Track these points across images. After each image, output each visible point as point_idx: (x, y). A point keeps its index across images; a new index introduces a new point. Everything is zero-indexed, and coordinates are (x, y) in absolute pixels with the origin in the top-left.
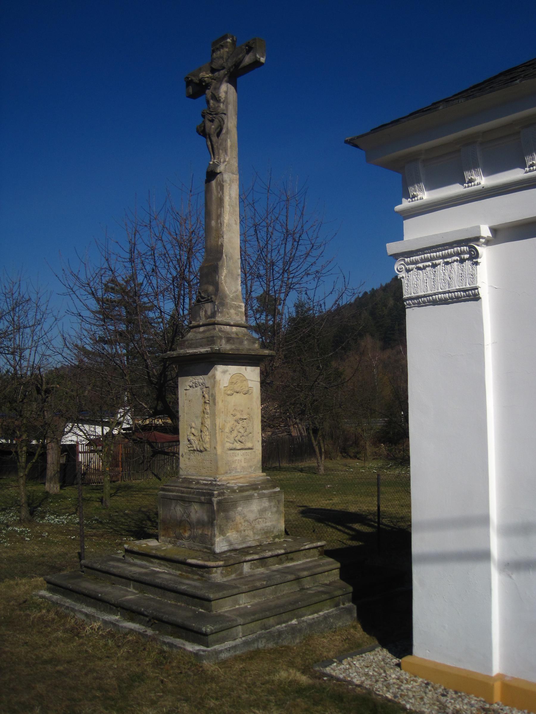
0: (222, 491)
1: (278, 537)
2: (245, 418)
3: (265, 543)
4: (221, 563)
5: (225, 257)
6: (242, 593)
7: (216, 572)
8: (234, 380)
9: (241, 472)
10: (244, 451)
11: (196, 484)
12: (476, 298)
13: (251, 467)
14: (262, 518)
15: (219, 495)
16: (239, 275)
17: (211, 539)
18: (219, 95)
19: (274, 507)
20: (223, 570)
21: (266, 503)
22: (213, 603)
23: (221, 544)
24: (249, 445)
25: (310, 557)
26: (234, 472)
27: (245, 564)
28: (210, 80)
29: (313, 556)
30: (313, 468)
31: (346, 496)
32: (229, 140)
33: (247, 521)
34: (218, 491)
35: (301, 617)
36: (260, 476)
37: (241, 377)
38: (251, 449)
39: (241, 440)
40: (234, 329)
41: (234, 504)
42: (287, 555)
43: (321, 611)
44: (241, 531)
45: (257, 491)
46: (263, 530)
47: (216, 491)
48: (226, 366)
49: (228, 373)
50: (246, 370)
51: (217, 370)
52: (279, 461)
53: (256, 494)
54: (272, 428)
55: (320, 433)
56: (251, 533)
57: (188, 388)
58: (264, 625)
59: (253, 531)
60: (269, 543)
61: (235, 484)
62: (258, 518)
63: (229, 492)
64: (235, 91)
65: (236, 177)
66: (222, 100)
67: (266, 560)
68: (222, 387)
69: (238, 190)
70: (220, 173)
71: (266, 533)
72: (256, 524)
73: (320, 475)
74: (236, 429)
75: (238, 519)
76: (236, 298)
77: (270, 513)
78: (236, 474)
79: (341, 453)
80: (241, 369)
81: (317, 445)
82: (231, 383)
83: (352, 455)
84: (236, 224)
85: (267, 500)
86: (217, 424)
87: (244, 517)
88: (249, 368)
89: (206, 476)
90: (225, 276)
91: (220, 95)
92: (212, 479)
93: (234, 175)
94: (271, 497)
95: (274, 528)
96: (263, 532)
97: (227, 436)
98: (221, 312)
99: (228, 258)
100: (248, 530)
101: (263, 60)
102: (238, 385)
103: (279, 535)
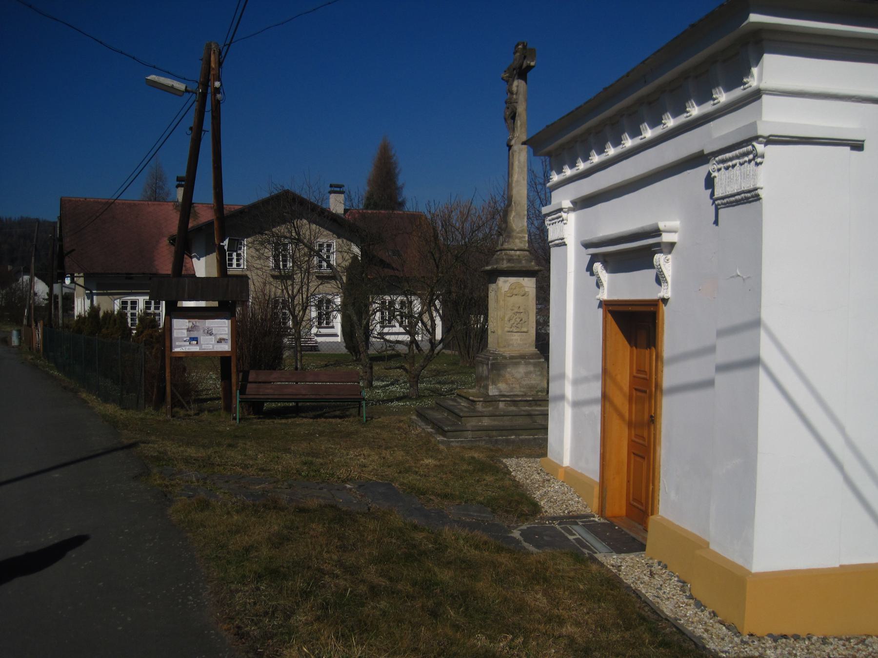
1: (541, 391)
2: (521, 311)
4: (481, 399)
6: (485, 416)
7: (479, 404)
9: (517, 347)
10: (519, 334)
12: (565, 244)
13: (526, 344)
15: (493, 359)
20: (483, 404)
21: (531, 368)
22: (463, 418)
24: (525, 330)
27: (500, 402)
32: (519, 121)
35: (519, 435)
38: (526, 332)
40: (518, 253)
41: (505, 366)
43: (536, 435)
44: (509, 384)
45: (525, 360)
49: (508, 282)
50: (523, 280)
56: (518, 386)
61: (509, 354)
64: (525, 84)
66: (514, 93)
67: (518, 403)
68: (503, 291)
70: (403, 184)
75: (507, 376)
76: (522, 231)
77: (534, 375)
80: (520, 280)
82: (510, 289)
88: (526, 279)
90: (514, 217)
92: (494, 350)
98: (507, 242)
99: (516, 205)
101: (532, 64)
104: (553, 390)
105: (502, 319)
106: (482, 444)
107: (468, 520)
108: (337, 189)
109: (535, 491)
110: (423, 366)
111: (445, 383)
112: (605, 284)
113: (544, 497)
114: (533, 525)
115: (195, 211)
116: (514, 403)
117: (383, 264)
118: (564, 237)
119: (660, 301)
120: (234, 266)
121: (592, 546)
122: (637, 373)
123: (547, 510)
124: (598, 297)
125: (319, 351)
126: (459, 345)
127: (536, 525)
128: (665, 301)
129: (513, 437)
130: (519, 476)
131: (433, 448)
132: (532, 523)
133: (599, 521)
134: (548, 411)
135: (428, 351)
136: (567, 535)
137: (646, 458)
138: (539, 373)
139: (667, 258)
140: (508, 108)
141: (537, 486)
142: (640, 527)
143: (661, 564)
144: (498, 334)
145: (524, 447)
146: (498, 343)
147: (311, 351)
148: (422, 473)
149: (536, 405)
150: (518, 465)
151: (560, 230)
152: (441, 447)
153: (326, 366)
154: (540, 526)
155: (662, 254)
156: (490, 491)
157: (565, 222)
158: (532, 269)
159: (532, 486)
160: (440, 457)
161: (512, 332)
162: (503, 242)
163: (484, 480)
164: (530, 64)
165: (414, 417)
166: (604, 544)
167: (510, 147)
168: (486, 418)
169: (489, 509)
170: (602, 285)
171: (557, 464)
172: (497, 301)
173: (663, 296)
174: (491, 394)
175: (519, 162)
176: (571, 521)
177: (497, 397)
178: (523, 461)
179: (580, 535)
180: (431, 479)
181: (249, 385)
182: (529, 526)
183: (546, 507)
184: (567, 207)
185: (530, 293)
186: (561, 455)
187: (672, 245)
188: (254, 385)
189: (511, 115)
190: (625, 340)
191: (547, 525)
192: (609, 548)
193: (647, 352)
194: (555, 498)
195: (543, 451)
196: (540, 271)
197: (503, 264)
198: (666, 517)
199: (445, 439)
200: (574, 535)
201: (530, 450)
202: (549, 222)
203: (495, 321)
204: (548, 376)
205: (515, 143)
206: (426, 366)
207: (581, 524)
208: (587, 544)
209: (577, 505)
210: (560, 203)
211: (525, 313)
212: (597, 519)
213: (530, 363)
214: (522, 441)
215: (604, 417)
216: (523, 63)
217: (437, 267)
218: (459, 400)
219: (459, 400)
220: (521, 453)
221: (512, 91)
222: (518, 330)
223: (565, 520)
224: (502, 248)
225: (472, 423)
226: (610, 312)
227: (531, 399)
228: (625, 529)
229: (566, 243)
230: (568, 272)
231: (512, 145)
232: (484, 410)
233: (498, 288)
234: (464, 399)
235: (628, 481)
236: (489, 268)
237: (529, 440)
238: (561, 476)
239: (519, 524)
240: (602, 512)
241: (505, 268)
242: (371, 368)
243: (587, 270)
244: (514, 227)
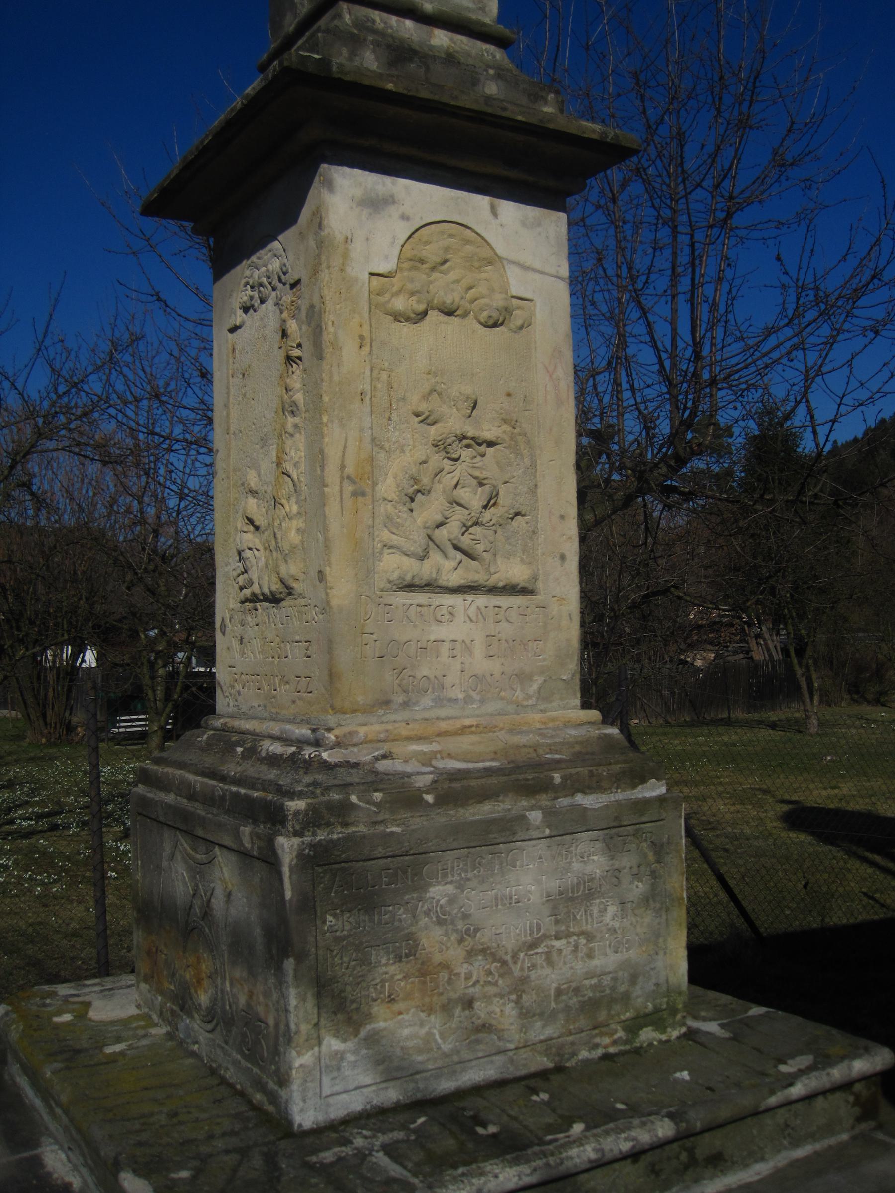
0: (335, 796)
2: (488, 435)
3: (584, 1054)
8: (431, 253)
9: (468, 700)
10: (482, 601)
11: (245, 756)
13: (523, 678)
14: (568, 935)
17: (276, 1052)
19: (636, 876)
23: (326, 1080)
25: (812, 1137)
26: (426, 701)
29: (829, 1129)
30: (797, 721)
31: (869, 781)
33: (483, 951)
34: (313, 795)
36: (568, 724)
37: (468, 242)
38: (525, 591)
39: (466, 541)
40: (441, 38)
42: (688, 1143)
45: (544, 800)
46: (577, 990)
47: (300, 795)
48: (388, 180)
49: (394, 211)
51: (329, 185)
52: (729, 707)
53: (535, 816)
54: (716, 645)
55: (809, 652)
57: (239, 316)
59: (517, 1002)
60: (606, 1057)
61: (427, 759)
62: (546, 937)
63: (378, 805)
68: (359, 271)
71: (591, 1006)
72: (534, 966)
73: (812, 735)
74: (438, 487)
77: (612, 909)
78: (443, 713)
79: (849, 692)
81: (803, 675)
83: (870, 697)
85: (598, 845)
86: (333, 454)
87: (472, 932)
88: (510, 210)
89: (290, 722)
92: (304, 731)
95: (634, 980)
96: (574, 1001)
97: (389, 518)
100: (487, 998)
102: (452, 276)
103: (657, 1010)
161: (430, 586)
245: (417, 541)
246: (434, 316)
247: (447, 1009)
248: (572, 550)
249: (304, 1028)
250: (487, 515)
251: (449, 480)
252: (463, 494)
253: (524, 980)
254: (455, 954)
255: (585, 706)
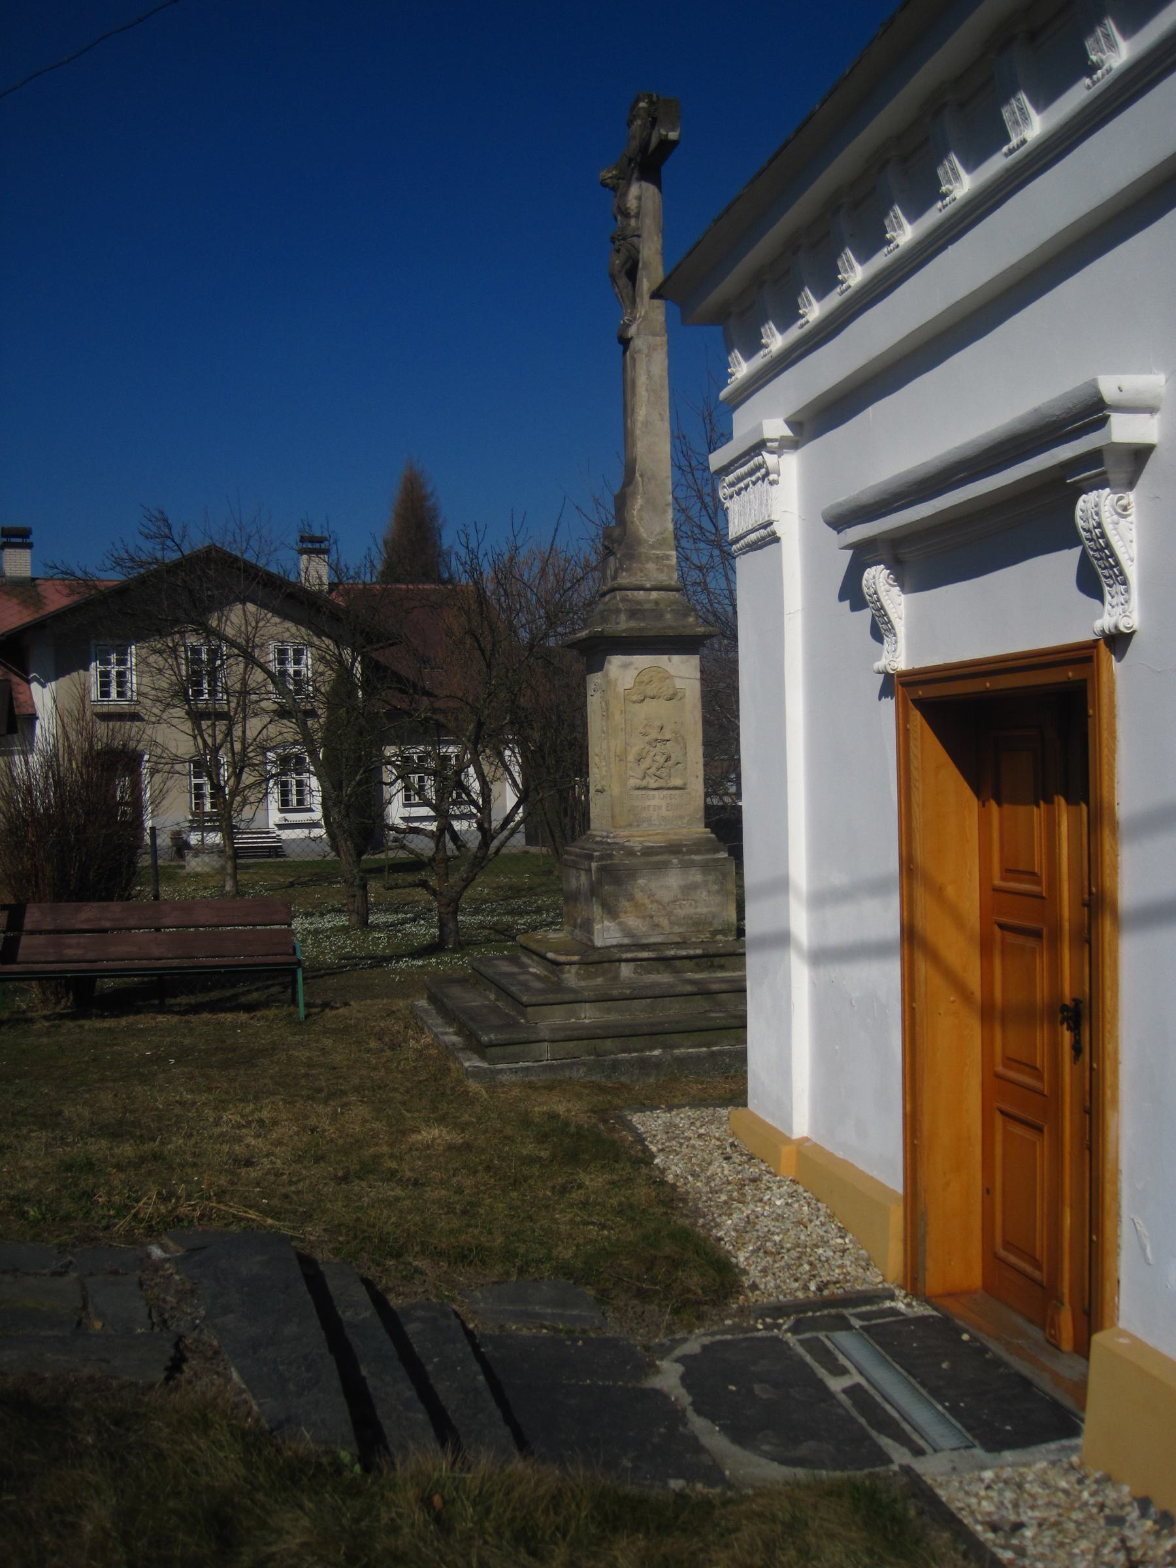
0: (609, 852)
1: (722, 932)
2: (667, 738)
4: (575, 958)
5: (639, 479)
6: (586, 1002)
7: (569, 971)
9: (660, 824)
10: (665, 792)
12: (774, 539)
13: (681, 817)
16: (668, 505)
18: (625, 205)
19: (715, 883)
20: (579, 969)
21: (696, 876)
24: (678, 782)
26: (645, 825)
27: (623, 964)
28: (615, 181)
32: (645, 280)
35: (672, 1047)
36: (697, 833)
39: (658, 773)
40: (654, 595)
41: (632, 873)
43: (715, 1044)
45: (680, 856)
46: (691, 918)
50: (670, 660)
51: (610, 662)
58: (595, 1049)
59: (669, 919)
61: (641, 843)
64: (656, 191)
65: (662, 340)
68: (620, 690)
69: (666, 362)
75: (639, 895)
76: (661, 543)
77: (705, 893)
80: (662, 660)
82: (638, 682)
84: (662, 420)
88: (676, 658)
90: (639, 511)
91: (628, 205)
92: (605, 834)
93: (658, 338)
94: (706, 867)
95: (714, 918)
96: (690, 921)
98: (627, 570)
99: (646, 479)
101: (673, 135)
104: (756, 922)
105: (622, 758)
106: (579, 1074)
107: (525, 1332)
108: (313, 545)
109: (720, 1215)
110: (468, 877)
111: (521, 914)
112: (900, 627)
113: (747, 1237)
114: (718, 1337)
115: (38, 594)
116: (666, 962)
117: (402, 684)
118: (773, 518)
119: (1102, 643)
120: (114, 695)
121: (905, 1419)
122: (1003, 879)
123: (758, 1281)
124: (879, 665)
125: (284, 856)
126: (553, 837)
127: (729, 1337)
128: (1118, 641)
129: (656, 1053)
130: (674, 1168)
131: (453, 1089)
132: (715, 1328)
133: (910, 1313)
134: (745, 980)
135: (476, 850)
136: (822, 1373)
137: (1046, 1129)
138: (716, 887)
139: (1123, 502)
140: (618, 251)
141: (724, 1197)
142: (1035, 1333)
143: (1152, 1510)
144: (611, 796)
145: (686, 1077)
146: (613, 817)
147: (269, 857)
148: (408, 1174)
149: (712, 967)
150: (669, 1128)
151: (761, 504)
152: (474, 1086)
153: (292, 884)
154: (741, 1336)
155: (1107, 490)
156: (593, 1224)
157: (772, 477)
158: (688, 632)
159: (710, 1199)
160: (466, 1117)
161: (645, 788)
162: (616, 571)
163: (580, 1186)
164: (667, 135)
165: (423, 1003)
166: (940, 1408)
167: (625, 342)
168: (587, 1005)
169: (590, 1292)
170: (892, 630)
171: (776, 1132)
172: (607, 714)
173: (1116, 627)
174: (598, 943)
175: (650, 376)
176: (829, 1315)
177: (615, 950)
178: (683, 1117)
179: (861, 1373)
180: (430, 1194)
181: (25, 940)
182: (707, 1340)
183: (754, 1272)
184: (776, 436)
185: (688, 693)
186: (785, 1107)
187: (1140, 455)
188: (40, 939)
189: (628, 265)
190: (966, 785)
191: (759, 1334)
192: (959, 1426)
193: (1038, 813)
194: (777, 1238)
195: (734, 1086)
196: (710, 636)
197: (618, 624)
198: (1151, 1342)
199: (485, 1065)
200: (841, 1371)
201: (702, 1083)
202: (728, 491)
203: (604, 763)
204: (740, 886)
205: (638, 334)
206: (473, 879)
207: (857, 1323)
208: (884, 1410)
209: (840, 1262)
210: (759, 429)
211: (677, 741)
212: (901, 1306)
213: (692, 864)
214: (681, 1061)
215: (913, 1009)
216: (650, 135)
217: (489, 666)
218: (525, 960)
219: (525, 960)
220: (678, 1094)
221: (627, 209)
222: (661, 783)
223: (810, 1314)
224: (615, 584)
225: (553, 1019)
226: (921, 704)
227: (699, 952)
228: (993, 1345)
229: (778, 535)
230: (786, 611)
231: (632, 338)
232: (583, 984)
233: (608, 682)
234: (535, 957)
235: (988, 1191)
236: (583, 634)
237: (698, 1059)
238: (788, 1168)
239: (678, 1336)
240: (913, 1283)
241: (624, 631)
242: (364, 887)
243: (842, 598)
244: (643, 532)
245: (640, 774)
246: (647, 700)
247: (644, 917)
248: (701, 773)
249: (598, 917)
250: (666, 764)
251: (652, 754)
252: (657, 758)
253: (671, 912)
254: (647, 901)
255: (706, 827)
